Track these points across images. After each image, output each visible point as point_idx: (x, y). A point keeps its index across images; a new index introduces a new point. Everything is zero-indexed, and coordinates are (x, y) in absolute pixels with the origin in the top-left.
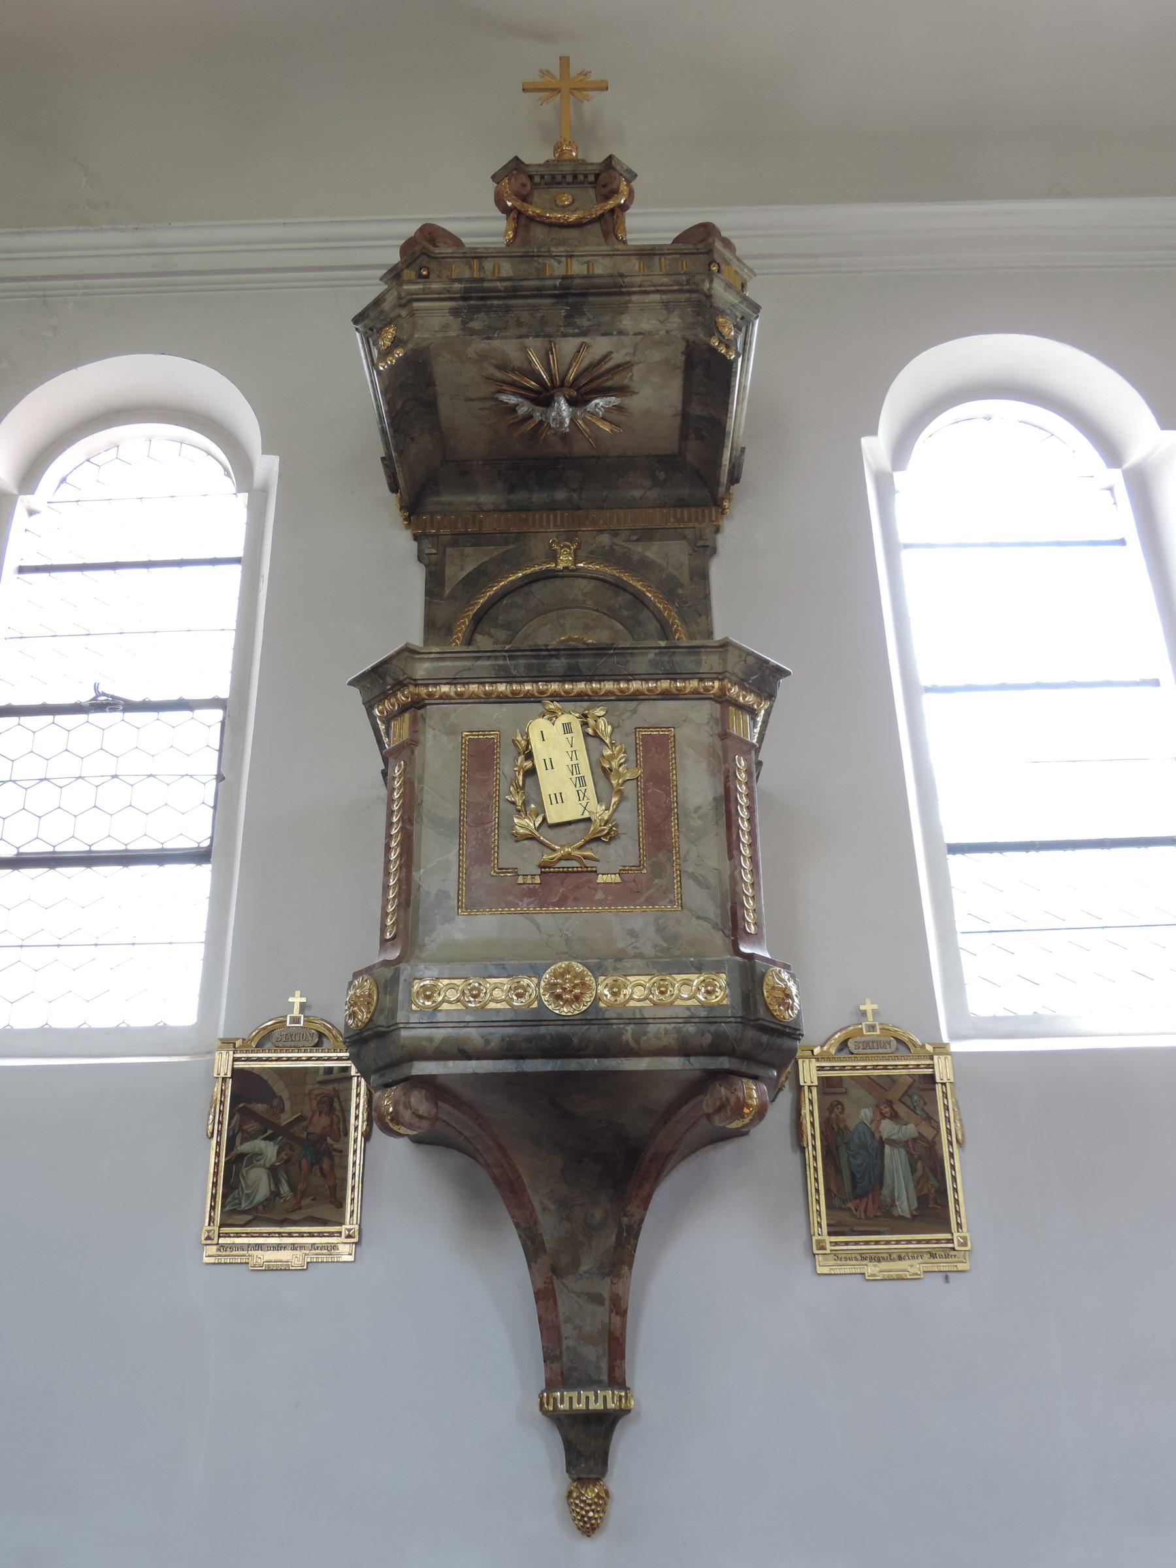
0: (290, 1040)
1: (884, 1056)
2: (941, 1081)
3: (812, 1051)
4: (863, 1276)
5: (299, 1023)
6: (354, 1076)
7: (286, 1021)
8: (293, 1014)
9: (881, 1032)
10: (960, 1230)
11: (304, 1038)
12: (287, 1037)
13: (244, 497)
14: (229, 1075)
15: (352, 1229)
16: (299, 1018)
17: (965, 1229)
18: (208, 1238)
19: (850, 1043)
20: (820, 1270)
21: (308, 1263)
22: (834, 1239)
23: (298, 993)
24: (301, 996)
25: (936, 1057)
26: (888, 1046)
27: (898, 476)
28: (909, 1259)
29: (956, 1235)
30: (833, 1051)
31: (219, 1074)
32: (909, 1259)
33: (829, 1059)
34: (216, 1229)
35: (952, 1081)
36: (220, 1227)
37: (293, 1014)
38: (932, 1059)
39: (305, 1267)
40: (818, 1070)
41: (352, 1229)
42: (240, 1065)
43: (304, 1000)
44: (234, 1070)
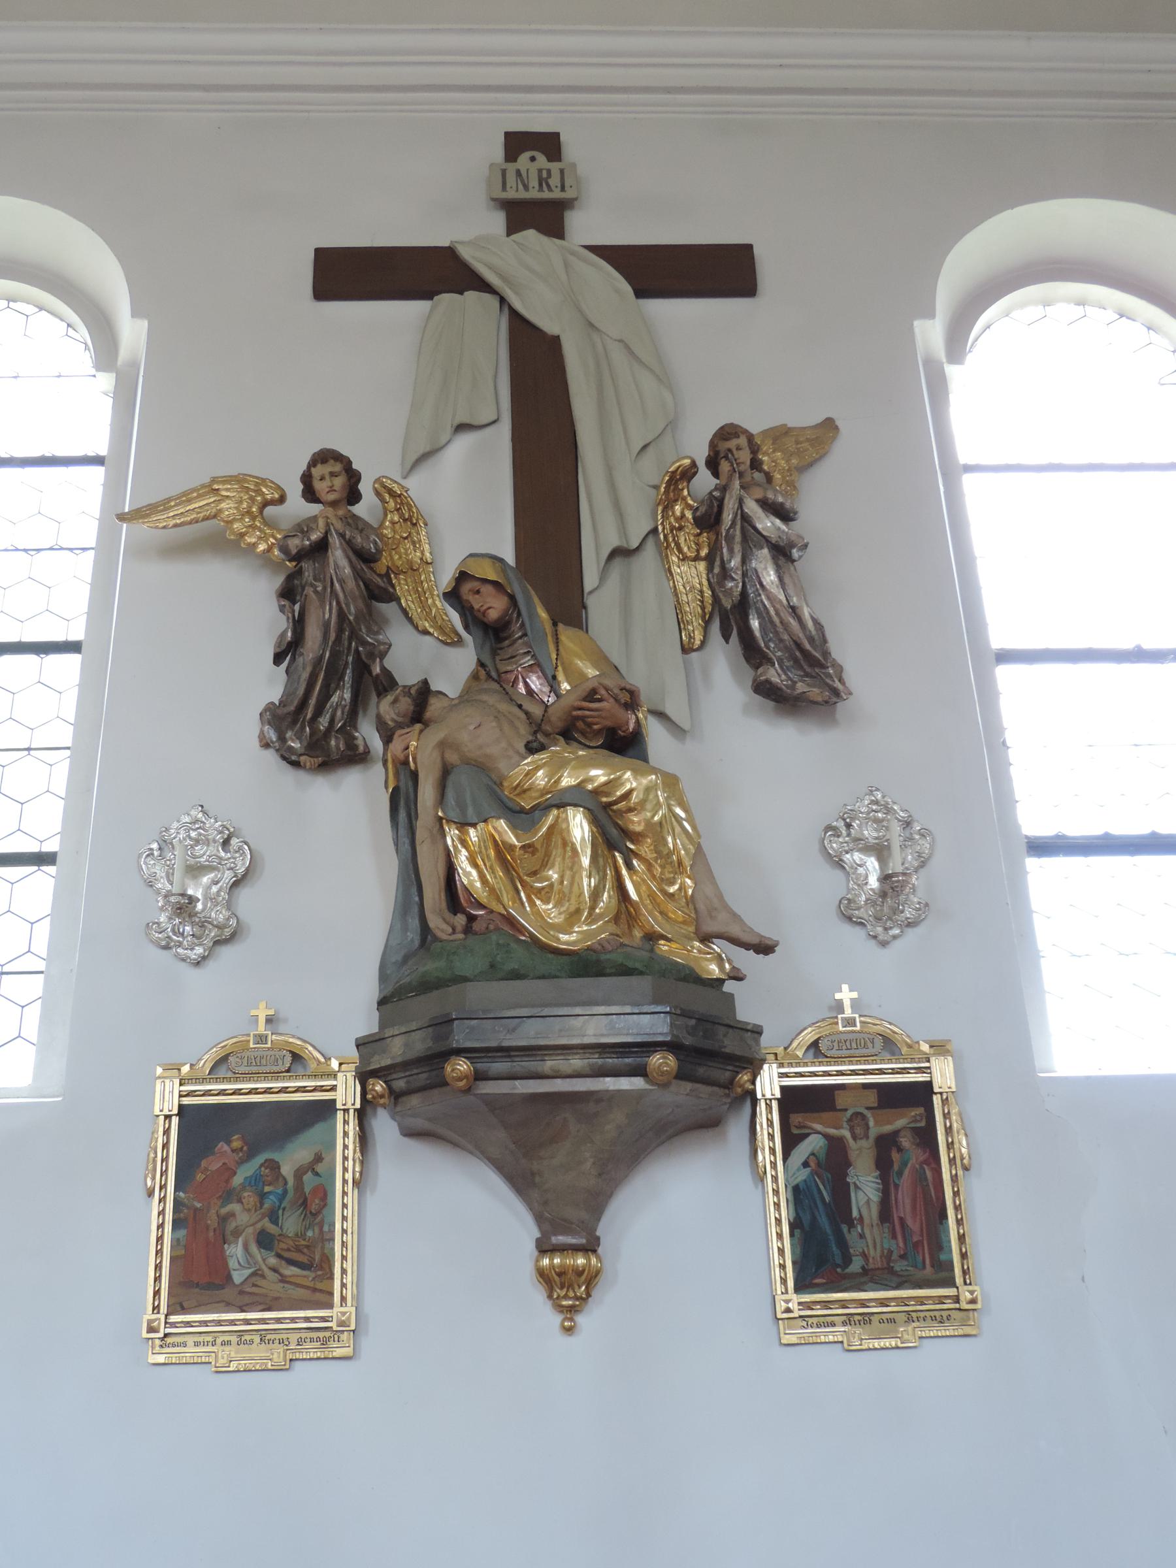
0: (844, 1047)
1: (865, 1058)
2: (343, 1107)
3: (179, 1070)
4: (840, 1345)
5: (855, 1025)
6: (340, 1110)
7: (249, 1041)
8: (844, 1013)
9: (861, 1027)
10: (344, 1305)
11: (863, 1046)
12: (841, 1045)
13: (106, 381)
14: (175, 1111)
15: (346, 1313)
16: (854, 1019)
17: (349, 1303)
18: (151, 1330)
19: (231, 1059)
20: (786, 1339)
21: (291, 1360)
22: (807, 1298)
23: (845, 987)
24: (850, 991)
25: (932, 1059)
26: (280, 1062)
27: (952, 371)
28: (855, 1324)
29: (962, 1288)
30: (800, 1053)
31: (161, 1111)
32: (855, 1324)
33: (203, 1081)
34: (162, 1317)
35: (954, 1089)
36: (166, 1316)
37: (844, 1013)
38: (929, 1061)
39: (287, 1367)
40: (779, 1077)
41: (346, 1313)
42: (186, 1101)
43: (855, 995)
44: (181, 1107)
